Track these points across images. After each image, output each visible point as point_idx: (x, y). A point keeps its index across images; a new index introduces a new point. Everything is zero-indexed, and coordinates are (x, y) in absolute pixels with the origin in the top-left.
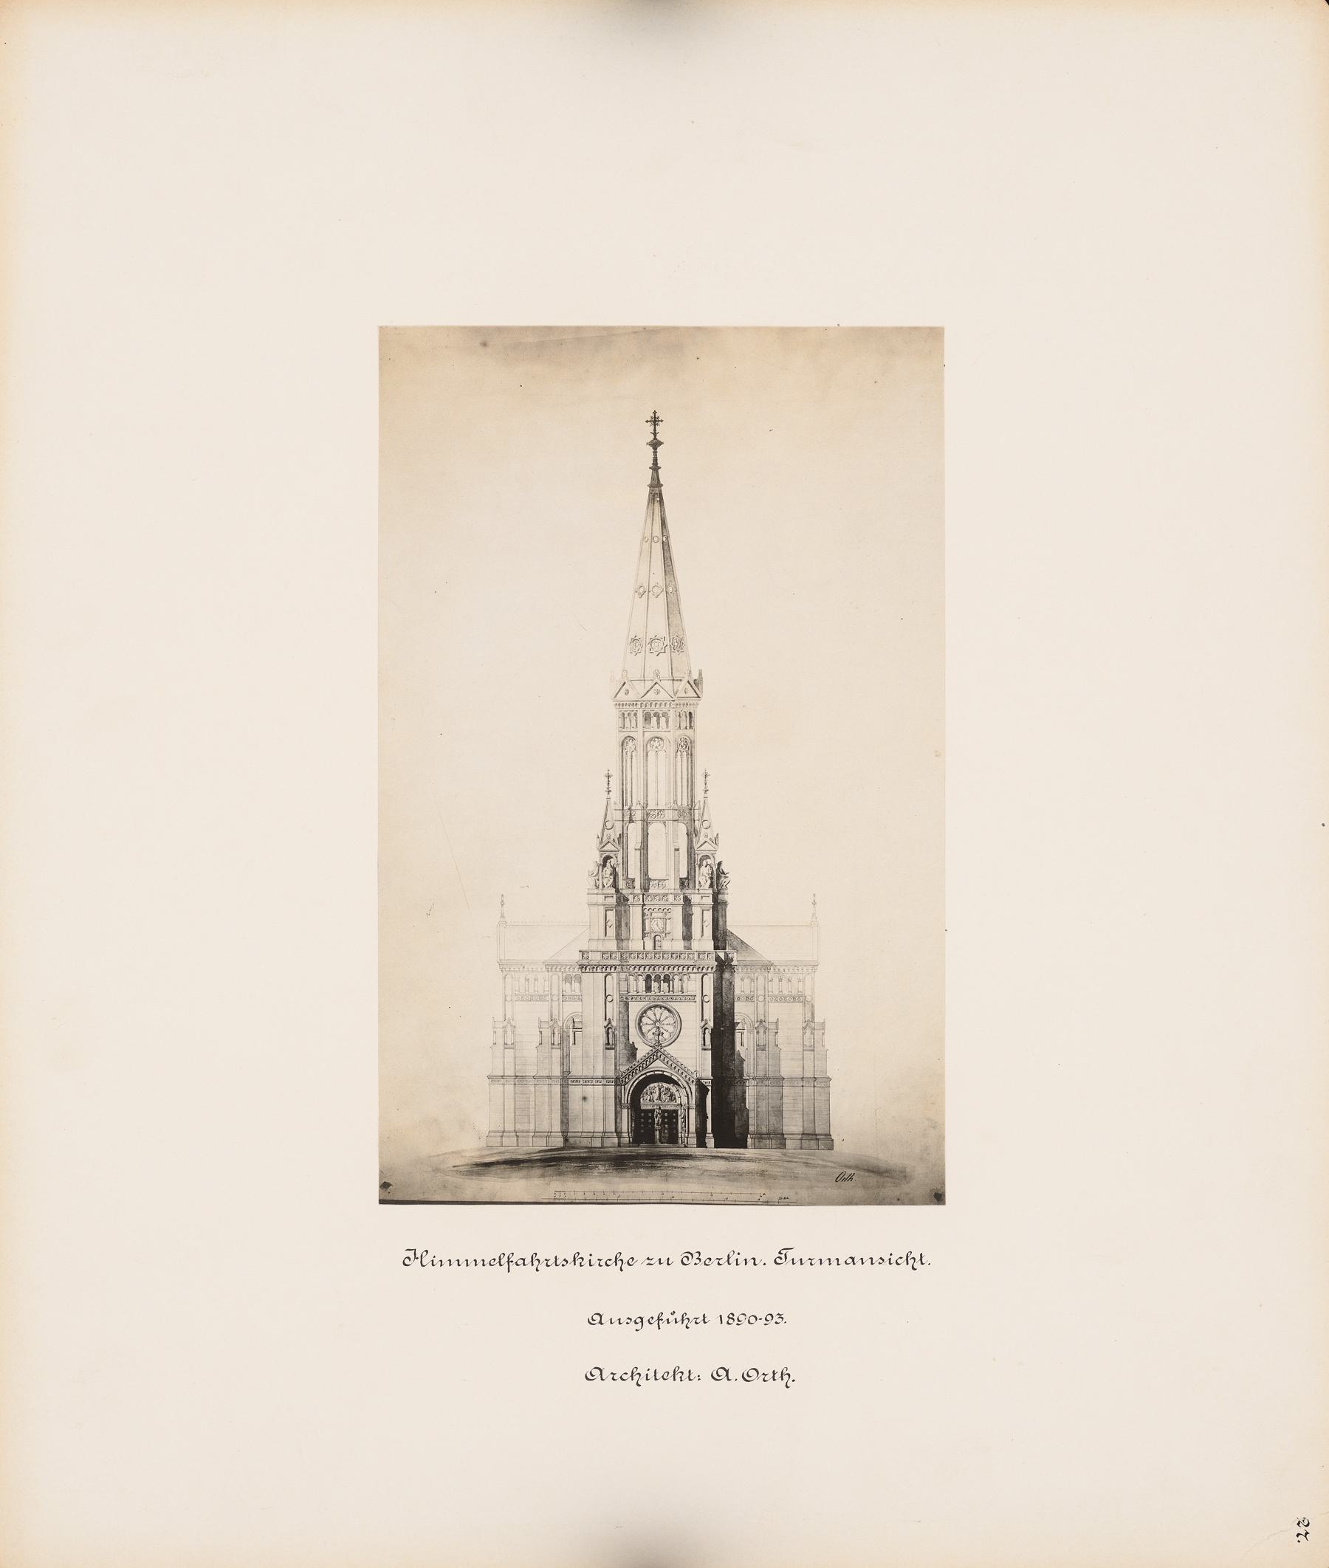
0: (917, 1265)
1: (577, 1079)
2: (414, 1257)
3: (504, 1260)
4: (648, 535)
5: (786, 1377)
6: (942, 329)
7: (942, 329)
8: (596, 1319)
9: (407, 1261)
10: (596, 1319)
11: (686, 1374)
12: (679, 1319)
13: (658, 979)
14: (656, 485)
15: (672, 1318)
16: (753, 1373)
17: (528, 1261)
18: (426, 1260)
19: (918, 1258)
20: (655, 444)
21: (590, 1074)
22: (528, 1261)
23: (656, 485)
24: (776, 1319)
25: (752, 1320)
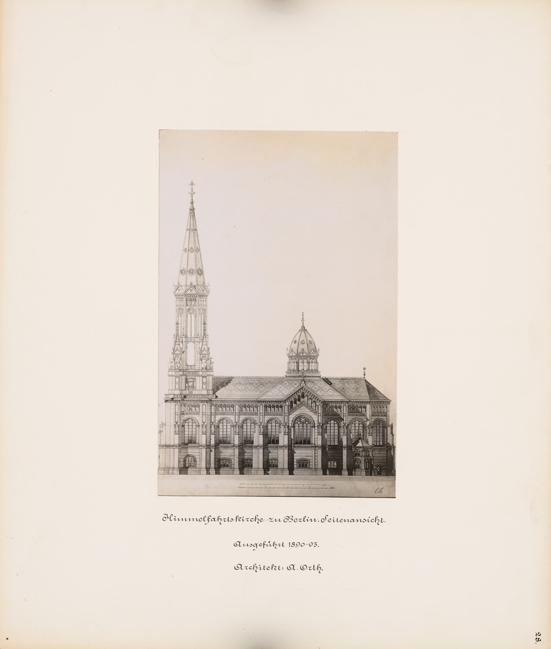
0: (380, 523)
1: (286, 447)
2: (167, 517)
3: (206, 519)
4: (188, 228)
5: (319, 569)
6: (395, 135)
7: (395, 135)
8: (238, 544)
9: (164, 519)
10: (238, 544)
11: (277, 567)
12: (272, 544)
13: (270, 406)
14: (192, 210)
15: (268, 544)
16: (305, 567)
17: (216, 519)
18: (172, 518)
19: (380, 520)
20: (192, 194)
21: (172, 444)
22: (216, 519)
23: (192, 210)
24: (314, 545)
25: (303, 545)
